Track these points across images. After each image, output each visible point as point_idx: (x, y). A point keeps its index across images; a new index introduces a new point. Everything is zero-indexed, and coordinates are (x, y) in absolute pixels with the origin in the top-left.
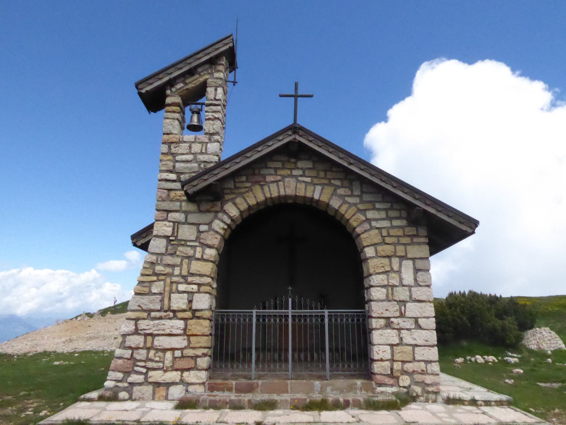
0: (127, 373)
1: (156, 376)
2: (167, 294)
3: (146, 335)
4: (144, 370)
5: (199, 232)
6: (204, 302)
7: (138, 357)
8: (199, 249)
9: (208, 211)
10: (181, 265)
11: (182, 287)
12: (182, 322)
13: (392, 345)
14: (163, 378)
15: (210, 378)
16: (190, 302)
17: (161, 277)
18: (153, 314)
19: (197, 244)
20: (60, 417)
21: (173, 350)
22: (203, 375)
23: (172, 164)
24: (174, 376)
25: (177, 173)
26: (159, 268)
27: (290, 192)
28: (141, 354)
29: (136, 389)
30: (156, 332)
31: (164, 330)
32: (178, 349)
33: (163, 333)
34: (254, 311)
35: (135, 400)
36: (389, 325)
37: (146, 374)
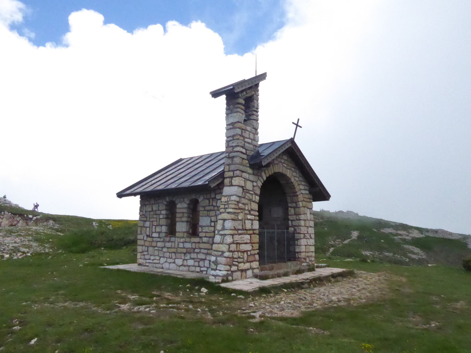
0: (230, 266)
1: (242, 266)
3: (237, 244)
4: (237, 263)
5: (253, 186)
6: (256, 225)
7: (235, 256)
8: (254, 195)
11: (249, 217)
13: (305, 245)
14: (245, 267)
15: (260, 265)
18: (240, 232)
19: (253, 193)
20: (344, 270)
21: (247, 251)
22: (258, 263)
23: (244, 143)
24: (247, 265)
26: (240, 205)
27: (281, 171)
29: (234, 274)
30: (241, 242)
31: (244, 241)
32: (249, 251)
33: (243, 242)
35: (235, 280)
37: (237, 266)
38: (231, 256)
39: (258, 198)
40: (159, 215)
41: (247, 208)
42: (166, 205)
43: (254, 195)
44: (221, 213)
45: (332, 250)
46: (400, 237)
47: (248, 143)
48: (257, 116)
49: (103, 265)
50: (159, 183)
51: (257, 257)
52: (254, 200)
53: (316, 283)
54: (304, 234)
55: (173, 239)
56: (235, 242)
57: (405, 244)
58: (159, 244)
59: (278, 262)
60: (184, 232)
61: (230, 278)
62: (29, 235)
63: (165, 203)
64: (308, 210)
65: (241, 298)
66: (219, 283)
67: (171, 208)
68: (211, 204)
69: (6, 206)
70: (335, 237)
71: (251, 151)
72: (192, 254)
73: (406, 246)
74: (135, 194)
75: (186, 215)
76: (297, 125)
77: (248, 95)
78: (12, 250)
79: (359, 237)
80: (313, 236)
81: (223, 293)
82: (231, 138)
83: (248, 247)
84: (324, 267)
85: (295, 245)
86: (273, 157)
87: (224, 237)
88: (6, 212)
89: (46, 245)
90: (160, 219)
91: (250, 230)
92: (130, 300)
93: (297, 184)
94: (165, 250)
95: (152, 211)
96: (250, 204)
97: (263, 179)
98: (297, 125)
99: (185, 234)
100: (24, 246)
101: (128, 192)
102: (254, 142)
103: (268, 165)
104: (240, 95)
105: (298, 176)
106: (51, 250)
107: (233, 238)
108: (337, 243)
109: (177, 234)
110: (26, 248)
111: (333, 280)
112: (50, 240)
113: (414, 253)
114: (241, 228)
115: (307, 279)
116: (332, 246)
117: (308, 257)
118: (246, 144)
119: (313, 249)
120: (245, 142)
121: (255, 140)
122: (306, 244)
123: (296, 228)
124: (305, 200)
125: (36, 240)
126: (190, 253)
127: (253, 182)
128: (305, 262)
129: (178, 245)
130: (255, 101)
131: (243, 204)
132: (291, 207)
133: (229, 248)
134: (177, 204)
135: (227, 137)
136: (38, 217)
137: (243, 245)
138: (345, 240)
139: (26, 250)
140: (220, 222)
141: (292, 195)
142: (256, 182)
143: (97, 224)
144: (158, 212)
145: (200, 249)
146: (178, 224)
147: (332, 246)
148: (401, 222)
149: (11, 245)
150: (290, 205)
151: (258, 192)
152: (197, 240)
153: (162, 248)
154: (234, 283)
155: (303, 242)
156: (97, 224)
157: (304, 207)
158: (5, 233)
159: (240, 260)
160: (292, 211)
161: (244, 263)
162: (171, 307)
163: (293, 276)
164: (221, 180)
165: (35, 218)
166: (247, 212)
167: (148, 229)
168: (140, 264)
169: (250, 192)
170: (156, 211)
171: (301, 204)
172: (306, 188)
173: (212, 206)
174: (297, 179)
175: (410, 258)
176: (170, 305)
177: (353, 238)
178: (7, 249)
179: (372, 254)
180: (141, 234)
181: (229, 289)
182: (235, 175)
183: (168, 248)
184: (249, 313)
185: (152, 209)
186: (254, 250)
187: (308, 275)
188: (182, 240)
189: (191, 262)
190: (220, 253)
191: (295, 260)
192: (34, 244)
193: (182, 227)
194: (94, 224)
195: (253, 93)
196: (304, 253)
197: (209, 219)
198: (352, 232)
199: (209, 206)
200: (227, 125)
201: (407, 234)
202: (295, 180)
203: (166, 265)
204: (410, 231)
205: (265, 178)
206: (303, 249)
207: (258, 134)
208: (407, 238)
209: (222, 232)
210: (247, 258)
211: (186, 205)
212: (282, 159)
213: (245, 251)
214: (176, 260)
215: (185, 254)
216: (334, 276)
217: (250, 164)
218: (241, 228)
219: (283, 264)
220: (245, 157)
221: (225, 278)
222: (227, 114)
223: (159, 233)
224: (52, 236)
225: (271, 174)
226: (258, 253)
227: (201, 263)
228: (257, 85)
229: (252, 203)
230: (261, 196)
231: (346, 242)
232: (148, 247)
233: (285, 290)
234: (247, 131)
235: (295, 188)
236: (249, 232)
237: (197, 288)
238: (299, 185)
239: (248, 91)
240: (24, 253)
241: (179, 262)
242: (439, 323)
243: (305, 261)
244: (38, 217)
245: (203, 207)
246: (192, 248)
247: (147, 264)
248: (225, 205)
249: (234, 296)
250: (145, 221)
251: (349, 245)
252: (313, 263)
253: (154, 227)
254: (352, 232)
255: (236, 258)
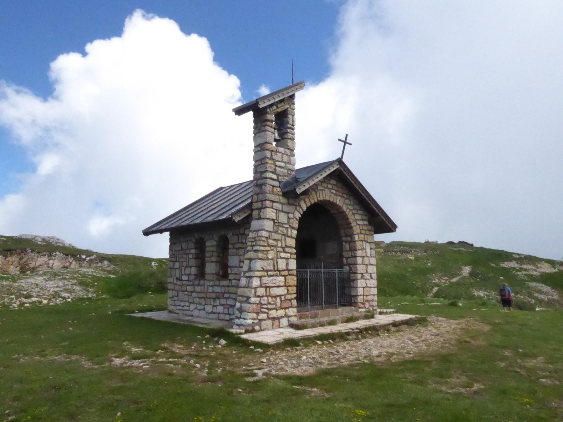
0: (257, 313)
1: (273, 313)
2: (275, 259)
3: (266, 287)
4: (266, 311)
5: (289, 218)
6: (293, 265)
7: (263, 302)
8: (289, 230)
9: (292, 205)
10: (281, 240)
11: (283, 255)
12: (283, 278)
13: (364, 288)
14: (277, 314)
15: (298, 312)
16: (287, 264)
17: (272, 248)
18: (270, 273)
19: (288, 226)
20: (413, 316)
21: (280, 296)
22: (295, 310)
23: (274, 167)
24: (281, 312)
25: (277, 175)
26: (271, 241)
27: (327, 198)
28: (265, 300)
29: (263, 323)
30: (271, 285)
32: (283, 295)
33: (275, 285)
34: (308, 270)
35: (264, 330)
36: (363, 277)
37: (268, 313)
38: (258, 302)
39: (295, 232)
40: (189, 254)
41: (279, 245)
42: (195, 243)
43: (289, 230)
44: (248, 251)
45: (436, 289)
46: (525, 272)
47: (280, 167)
48: (293, 134)
49: (135, 313)
50: (183, 220)
51: (295, 302)
52: (289, 234)
53: (369, 334)
54: (362, 274)
55: (202, 282)
56: (263, 285)
57: (532, 281)
58: (189, 288)
59: (326, 308)
60: (214, 274)
61: (257, 328)
62: (74, 278)
63: (194, 240)
64: (368, 244)
65: (258, 352)
66: (241, 334)
67: (201, 247)
68: (240, 241)
69: (59, 246)
70: (440, 274)
71: (285, 176)
72: (221, 300)
73: (534, 284)
74: (161, 231)
75: (215, 254)
76: (345, 142)
77: (279, 110)
78: (52, 295)
79: (471, 274)
80: (375, 276)
81: (242, 346)
82: (259, 163)
83: (282, 291)
84: (390, 313)
85: (351, 287)
86: (316, 180)
87: (249, 280)
88: (58, 253)
89: (90, 290)
90: (189, 258)
91: (284, 270)
92: (130, 353)
93: (351, 213)
94: (194, 295)
95: (182, 249)
96: (285, 240)
97: (302, 210)
98: (345, 142)
99: (215, 276)
100: (66, 291)
101: (154, 229)
102: (288, 166)
103: (306, 193)
104: (268, 110)
105: (352, 203)
106: (95, 295)
107: (260, 280)
108: (444, 281)
109: (207, 277)
110: (68, 293)
111: (393, 329)
112: (96, 284)
113: (540, 292)
114: (272, 268)
115: (357, 329)
116: (436, 285)
117: (367, 301)
118: (278, 169)
119: (375, 291)
120: (276, 166)
121: (290, 163)
122: (365, 285)
123: (351, 266)
124: (363, 232)
125: (81, 283)
126: (219, 298)
127: (288, 213)
128: (363, 308)
129: (208, 288)
130: (290, 116)
131: (275, 240)
132: (346, 242)
133: (256, 292)
134: (206, 242)
135: (256, 161)
136: (92, 257)
137: (274, 289)
138: (453, 277)
139: (66, 295)
140: (247, 262)
141: (346, 226)
142: (293, 213)
143: (157, 264)
144: (187, 251)
145: (230, 293)
146: (207, 265)
147: (436, 285)
148: (528, 254)
149: (52, 289)
150: (344, 239)
151: (296, 225)
152: (225, 283)
153: (192, 292)
154: (260, 333)
155: (361, 283)
156: (157, 264)
157: (362, 241)
158: (49, 276)
159: (270, 306)
160: (347, 246)
161: (277, 310)
162: (170, 362)
163: (341, 325)
164: (250, 212)
165: (88, 258)
166: (280, 249)
167: (178, 271)
168: (170, 312)
169: (284, 226)
170: (185, 250)
171: (356, 237)
172: (364, 217)
173: (242, 243)
174: (351, 207)
175: (535, 298)
176: (170, 360)
177: (464, 274)
178: (47, 294)
179: (487, 295)
180: (171, 276)
181: (248, 341)
182: (263, 207)
183: (198, 292)
184: (253, 370)
185: (182, 248)
186: (290, 294)
187: (362, 323)
188: (211, 283)
189: (220, 309)
190: (245, 299)
191: (350, 305)
192: (78, 288)
193: (211, 268)
194: (153, 264)
195: (287, 106)
196: (362, 297)
197: (239, 259)
198: (463, 267)
199: (239, 243)
200: (255, 147)
201: (534, 268)
202: (348, 208)
203: (196, 313)
204: (539, 265)
205: (305, 208)
206: (360, 291)
207: (294, 156)
208: (535, 273)
209: (247, 274)
210: (281, 304)
211: (215, 243)
212: (330, 184)
213: (278, 296)
214: (206, 307)
215: (214, 299)
216: (395, 324)
217: (283, 193)
218: (272, 268)
219: (331, 311)
220: (276, 184)
221: (250, 328)
222: (255, 134)
223: (189, 275)
224: (98, 279)
225: (313, 202)
226: (295, 298)
227: (231, 311)
228: (292, 97)
229: (287, 238)
230: (298, 230)
231: (454, 280)
232: (178, 291)
233: (319, 342)
234: (279, 152)
235: (348, 219)
236: (283, 273)
237: (215, 339)
238: (353, 214)
239: (279, 105)
240: (64, 298)
241: (209, 308)
242: (484, 385)
243: (362, 306)
244: (92, 257)
245: (232, 244)
246: (221, 293)
247: (177, 311)
248: (252, 242)
249: (252, 349)
250: (175, 262)
251: (458, 284)
252: (375, 308)
253: (183, 268)
254: (463, 267)
255: (265, 304)
